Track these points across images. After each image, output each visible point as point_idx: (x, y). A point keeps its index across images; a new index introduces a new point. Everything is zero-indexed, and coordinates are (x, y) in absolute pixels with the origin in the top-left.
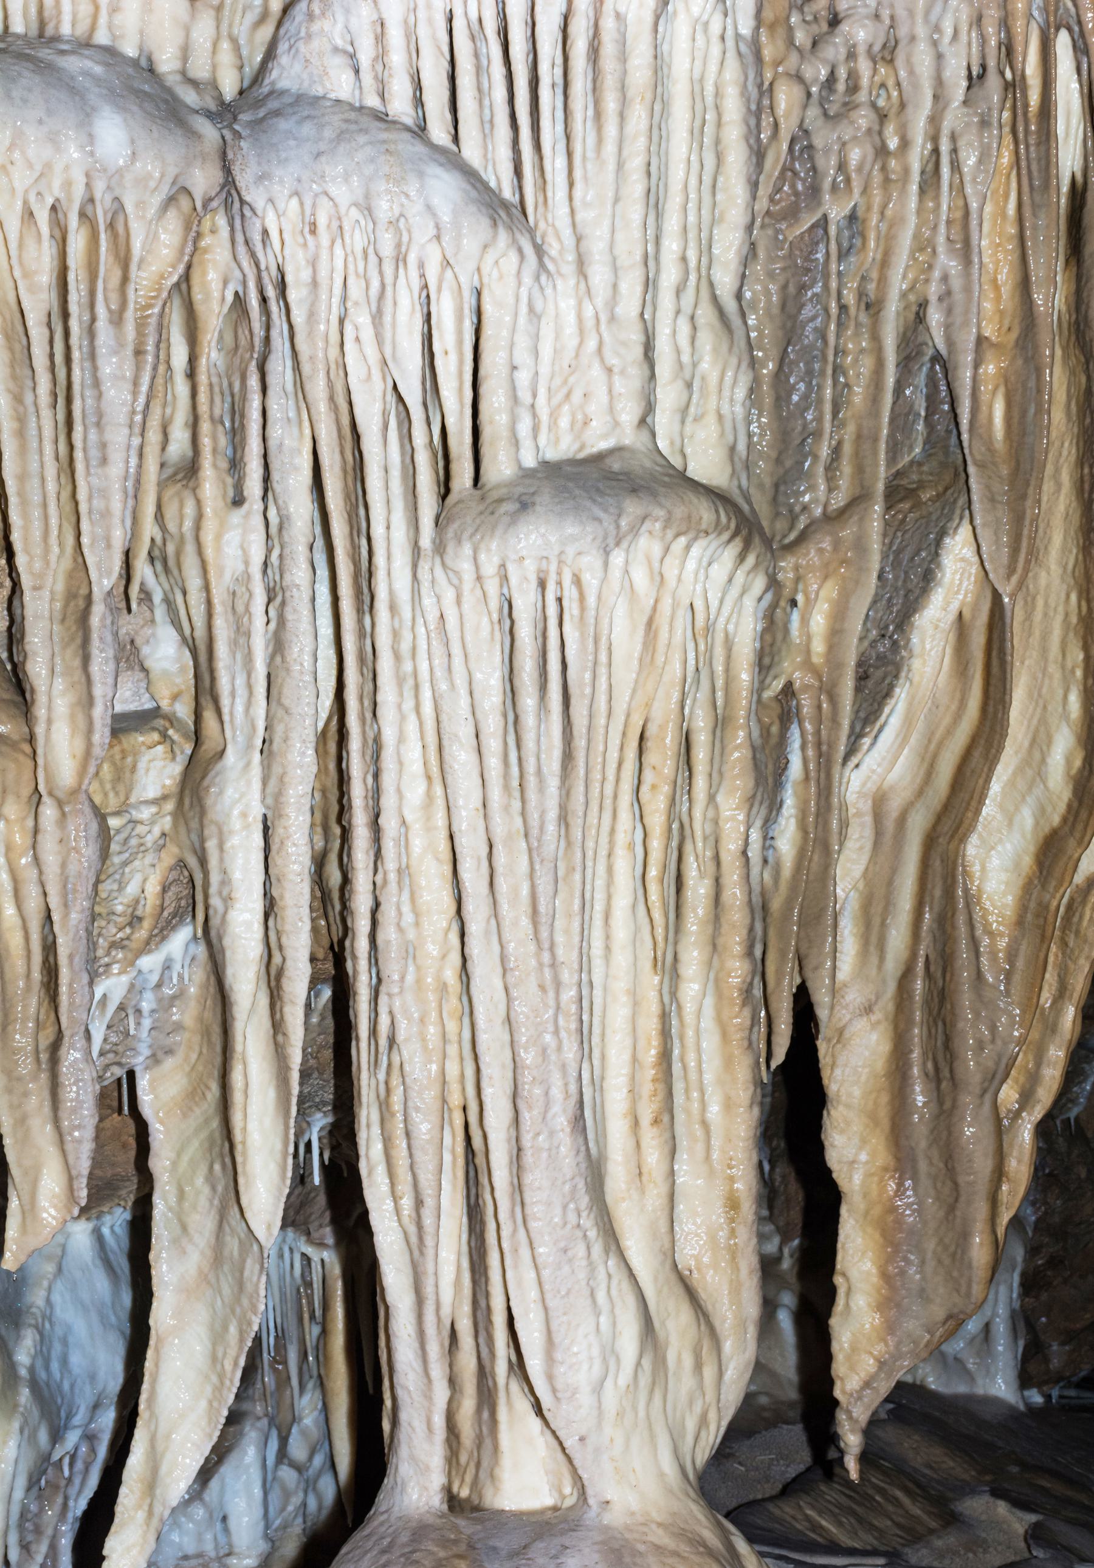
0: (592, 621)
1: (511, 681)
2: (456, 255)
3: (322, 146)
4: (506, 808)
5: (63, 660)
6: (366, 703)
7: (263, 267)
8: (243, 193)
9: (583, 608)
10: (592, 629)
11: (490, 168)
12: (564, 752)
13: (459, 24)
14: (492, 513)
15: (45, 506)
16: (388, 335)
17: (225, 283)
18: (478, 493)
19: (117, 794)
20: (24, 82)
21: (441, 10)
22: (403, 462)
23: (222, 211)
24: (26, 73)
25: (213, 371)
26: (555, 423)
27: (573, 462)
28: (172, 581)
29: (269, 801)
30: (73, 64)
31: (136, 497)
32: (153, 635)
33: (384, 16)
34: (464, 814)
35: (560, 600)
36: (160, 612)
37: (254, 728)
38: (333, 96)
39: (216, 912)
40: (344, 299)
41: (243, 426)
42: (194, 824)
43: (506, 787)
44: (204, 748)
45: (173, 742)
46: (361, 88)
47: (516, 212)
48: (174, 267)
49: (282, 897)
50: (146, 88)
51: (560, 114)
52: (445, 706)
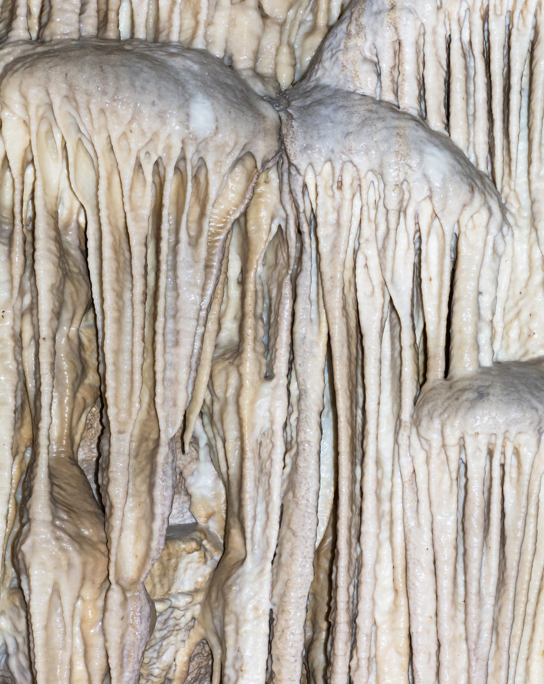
0: (526, 483)
1: (463, 523)
2: (442, 210)
3: (351, 128)
4: (453, 618)
5: (134, 485)
6: (353, 532)
7: (301, 210)
8: (292, 158)
9: (520, 472)
10: (525, 489)
11: (471, 148)
12: (499, 579)
13: (455, 46)
14: (457, 399)
15: (132, 373)
16: (389, 265)
17: (272, 219)
18: (447, 383)
19: (162, 585)
20: (144, 75)
21: (443, 36)
22: (392, 355)
23: (274, 169)
24: (146, 69)
25: (258, 281)
26: (507, 334)
27: (518, 364)
28: (216, 431)
29: (276, 600)
30: (178, 63)
31: (197, 370)
32: (197, 469)
33: (401, 38)
34: (420, 619)
35: (503, 466)
36: (203, 453)
37: (268, 544)
38: (360, 91)
39: (229, 679)
40: (359, 236)
41: (277, 322)
42: (218, 613)
43: (454, 602)
44: (230, 556)
45: (206, 550)
46: (381, 87)
47: (488, 181)
48: (237, 206)
49: (280, 672)
50: (229, 82)
51: (524, 111)
52: (412, 538)
